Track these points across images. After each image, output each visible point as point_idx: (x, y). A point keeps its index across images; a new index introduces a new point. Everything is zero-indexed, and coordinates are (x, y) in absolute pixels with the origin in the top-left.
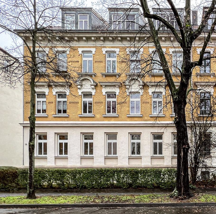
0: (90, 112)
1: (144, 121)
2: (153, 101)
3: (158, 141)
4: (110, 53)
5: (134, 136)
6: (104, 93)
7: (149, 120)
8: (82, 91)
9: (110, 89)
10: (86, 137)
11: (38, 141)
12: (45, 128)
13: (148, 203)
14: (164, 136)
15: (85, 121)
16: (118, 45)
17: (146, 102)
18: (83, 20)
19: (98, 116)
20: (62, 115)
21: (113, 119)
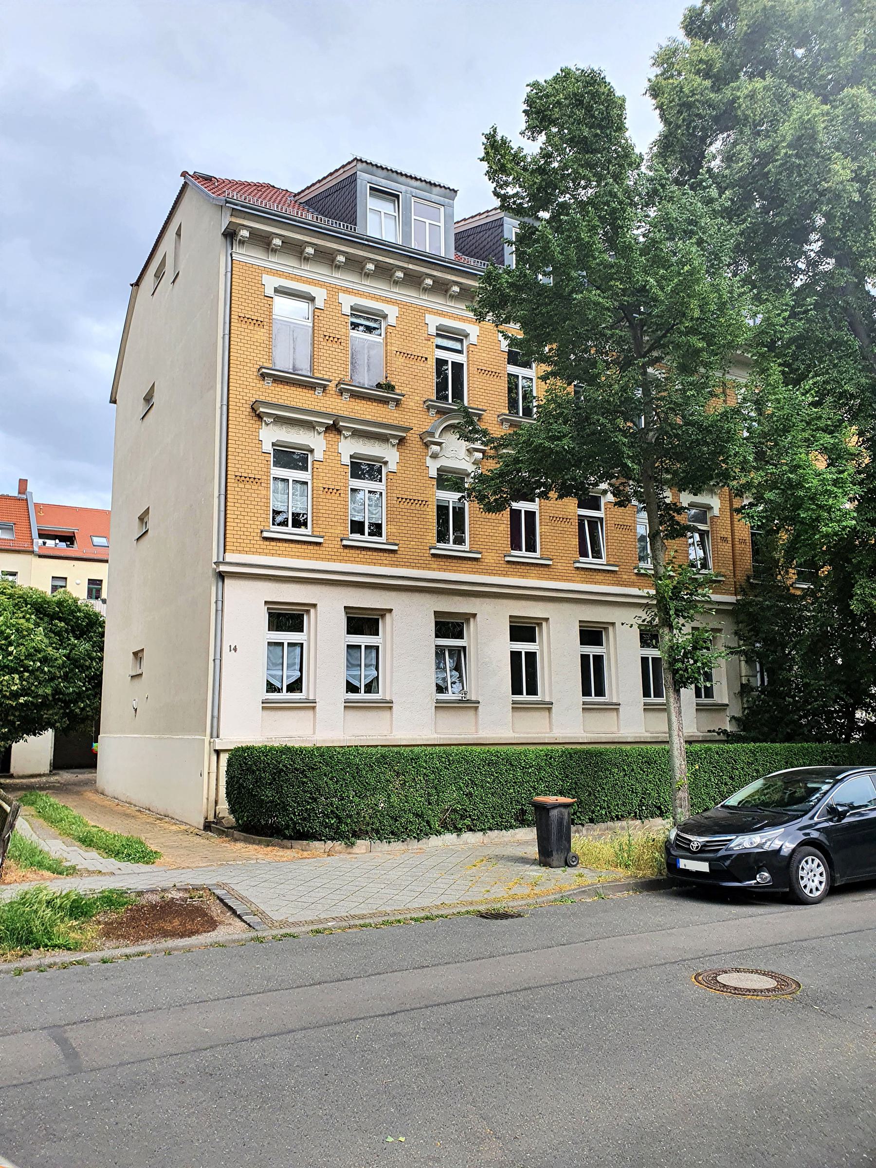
0: (459, 541)
1: (621, 585)
2: (272, 476)
3: (523, 647)
4: (367, 320)
5: (523, 631)
6: (268, 448)
7: (632, 585)
8: (438, 463)
9: (364, 445)
10: (94, 596)
11: (538, 647)
12: (487, 600)
13: (824, 879)
14: (544, 634)
15: (450, 571)
16: (398, 297)
17: (248, 479)
18: (428, 221)
19: (490, 558)
20: (365, 539)
21: (535, 571)
